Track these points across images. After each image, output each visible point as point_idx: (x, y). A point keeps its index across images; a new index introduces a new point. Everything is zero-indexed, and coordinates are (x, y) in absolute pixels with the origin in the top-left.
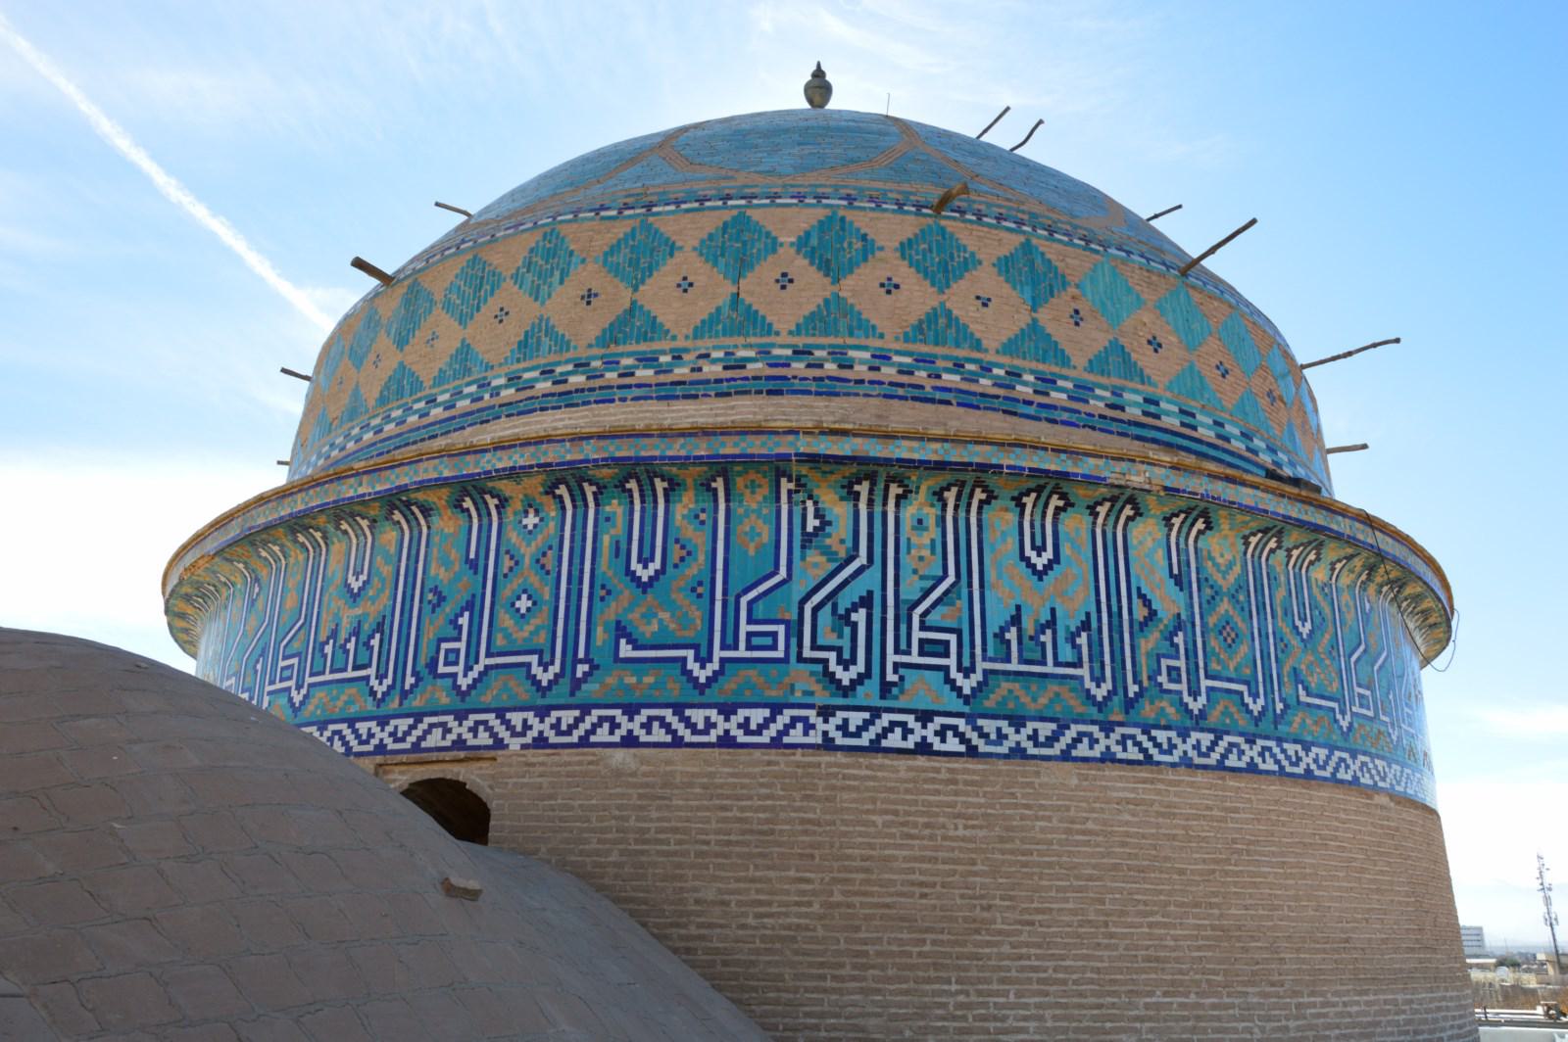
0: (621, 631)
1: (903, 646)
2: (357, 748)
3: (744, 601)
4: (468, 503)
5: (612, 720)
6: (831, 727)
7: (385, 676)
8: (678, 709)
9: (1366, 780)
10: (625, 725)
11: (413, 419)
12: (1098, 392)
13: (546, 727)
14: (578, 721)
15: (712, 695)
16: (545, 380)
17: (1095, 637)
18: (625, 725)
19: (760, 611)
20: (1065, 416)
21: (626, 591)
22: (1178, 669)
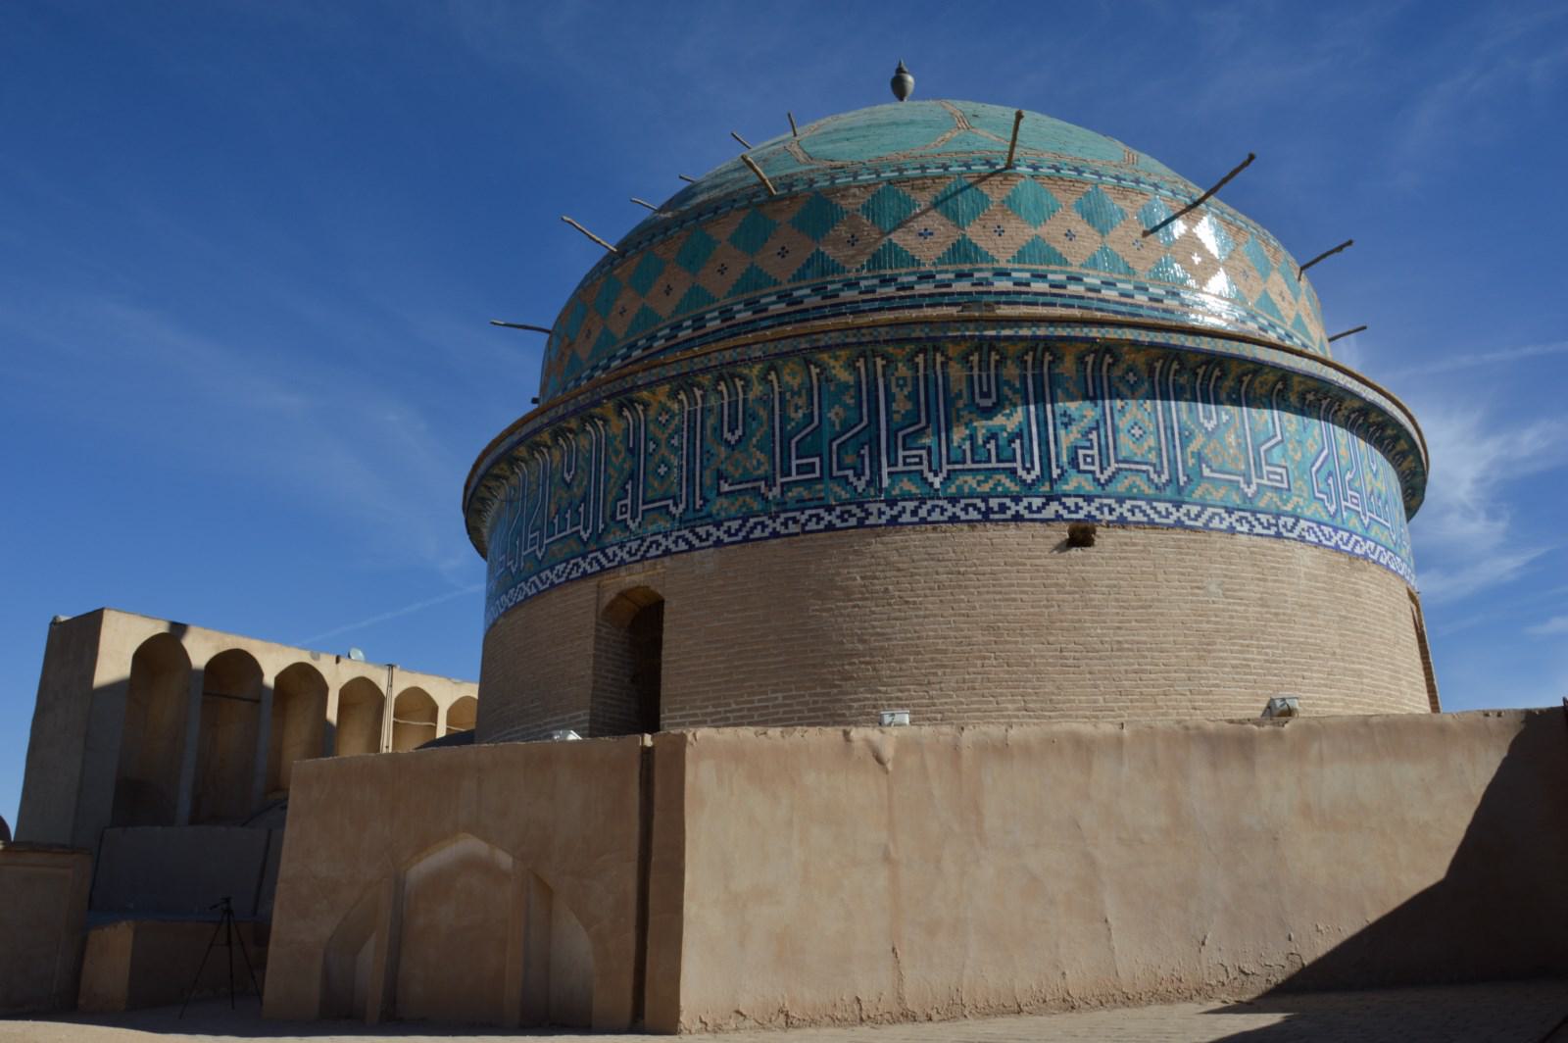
0: (720, 476)
1: (917, 460)
2: (608, 565)
5: (730, 535)
6: (1119, 510)
7: (637, 517)
8: (1149, 500)
9: (1392, 567)
10: (1021, 508)
12: (660, 334)
15: (1109, 489)
16: (816, 295)
17: (1027, 444)
21: (723, 451)
22: (1092, 457)
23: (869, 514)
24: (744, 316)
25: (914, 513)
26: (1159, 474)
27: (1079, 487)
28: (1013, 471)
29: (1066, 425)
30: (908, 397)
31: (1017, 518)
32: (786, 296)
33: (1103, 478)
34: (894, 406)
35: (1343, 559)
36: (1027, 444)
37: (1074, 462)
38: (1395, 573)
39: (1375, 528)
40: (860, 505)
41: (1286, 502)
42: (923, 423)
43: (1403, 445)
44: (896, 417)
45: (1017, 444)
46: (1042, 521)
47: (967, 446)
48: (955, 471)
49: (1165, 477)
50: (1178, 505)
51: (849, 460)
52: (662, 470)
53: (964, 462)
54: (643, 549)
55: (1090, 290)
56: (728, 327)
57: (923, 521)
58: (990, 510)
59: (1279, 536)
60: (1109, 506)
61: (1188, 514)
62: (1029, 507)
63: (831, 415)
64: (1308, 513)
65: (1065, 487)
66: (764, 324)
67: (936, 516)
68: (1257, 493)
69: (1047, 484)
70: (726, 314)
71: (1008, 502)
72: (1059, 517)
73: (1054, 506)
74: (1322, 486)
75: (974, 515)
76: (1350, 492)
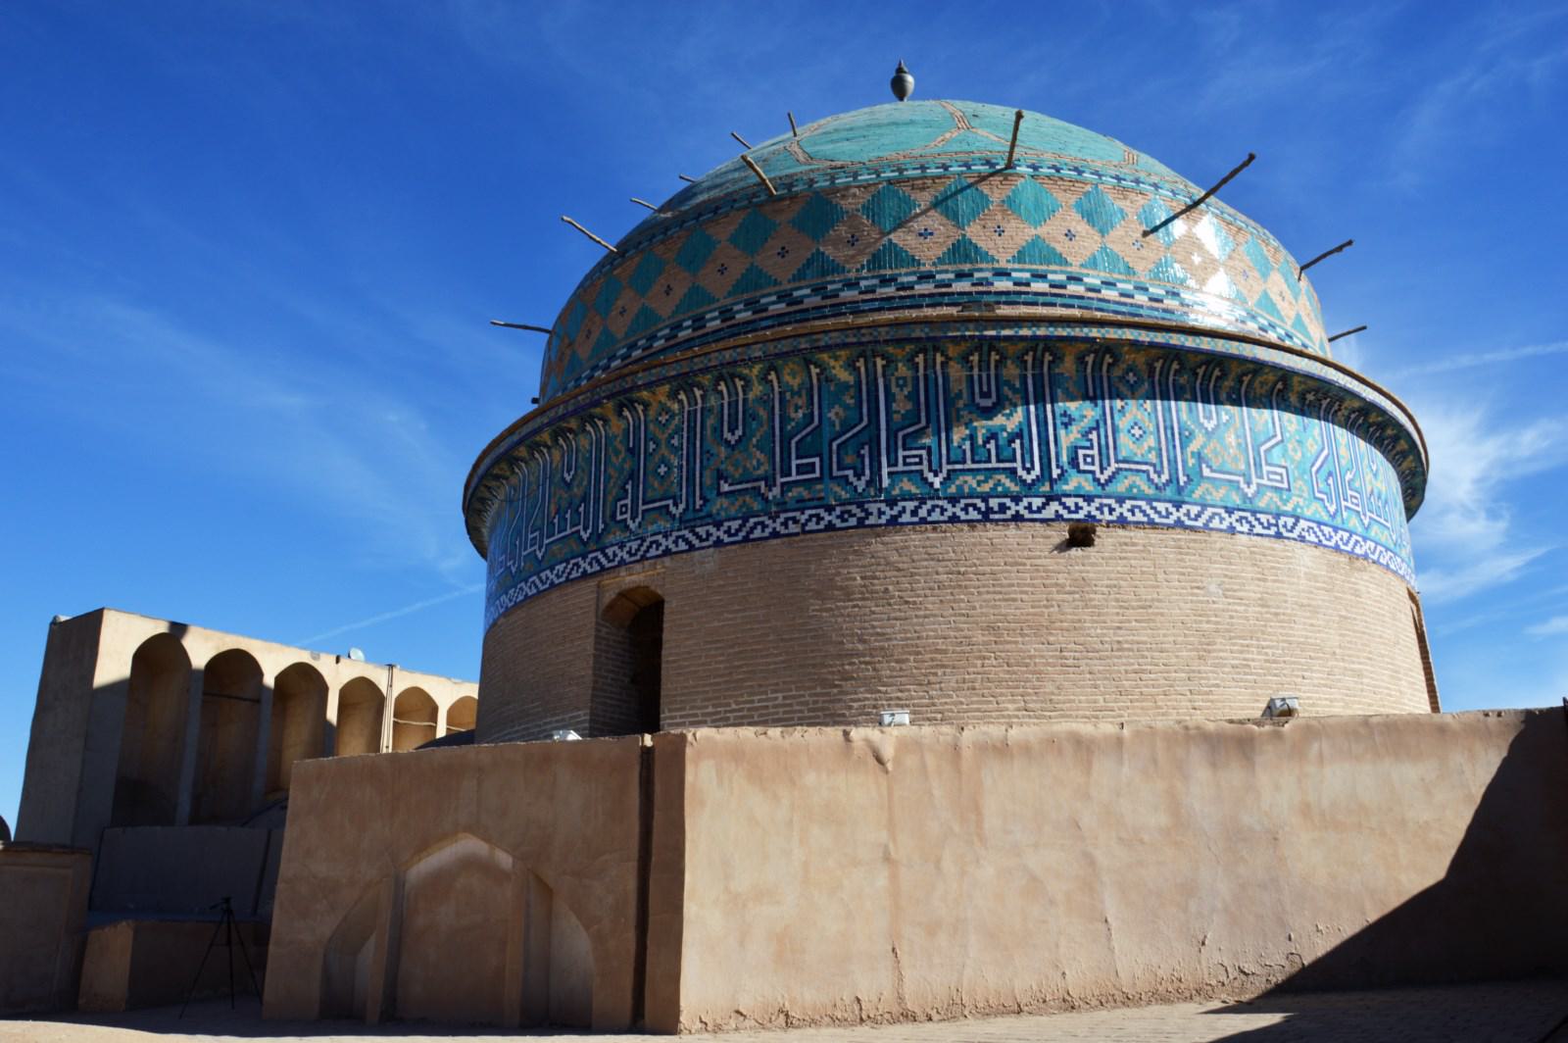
1: (917, 460)
7: (637, 517)
8: (1149, 500)
9: (1392, 566)
12: (660, 334)
15: (1109, 489)
17: (1027, 444)
22: (1092, 457)
23: (869, 514)
24: (744, 316)
25: (914, 513)
26: (1159, 474)
27: (1079, 487)
28: (1013, 471)
29: (1066, 425)
31: (1017, 518)
32: (786, 296)
33: (1103, 478)
35: (1343, 559)
36: (1027, 444)
37: (1074, 462)
38: (1395, 572)
39: (1375, 527)
40: (860, 505)
41: (1286, 502)
45: (1017, 444)
47: (967, 446)
48: (955, 471)
49: (1165, 477)
50: (1178, 506)
51: (848, 460)
52: (662, 470)
53: (964, 462)
54: (643, 548)
57: (923, 521)
58: (990, 510)
59: (1279, 536)
60: (1109, 506)
61: (1188, 514)
62: (1029, 507)
63: (832, 415)
64: (1308, 513)
65: (1065, 487)
67: (936, 516)
68: (1257, 492)
69: (1047, 484)
70: (726, 314)
72: (1058, 517)
73: (1054, 506)
74: (1322, 486)
75: (974, 515)
76: (1349, 492)
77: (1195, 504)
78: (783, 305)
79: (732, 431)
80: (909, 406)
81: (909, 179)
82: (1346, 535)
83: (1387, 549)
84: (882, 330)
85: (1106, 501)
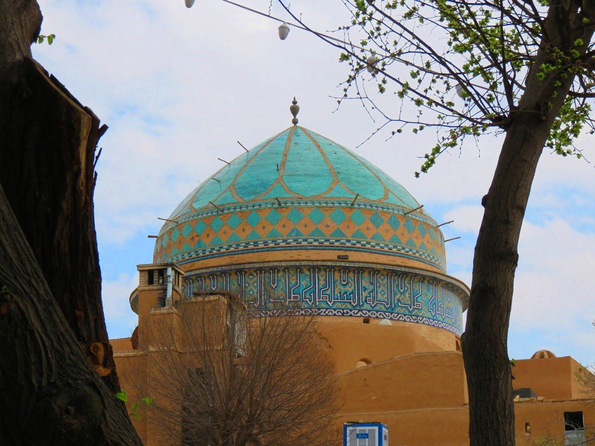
0: (399, 301)
3: (292, 290)
4: (187, 281)
8: (384, 312)
9: (451, 330)
11: (428, 258)
12: (241, 245)
13: (352, 313)
14: (397, 316)
15: (375, 308)
17: (354, 295)
18: (303, 312)
19: (294, 292)
20: (217, 255)
23: (313, 312)
24: (272, 245)
25: (325, 312)
26: (387, 304)
27: (367, 308)
28: (350, 303)
29: (364, 290)
30: (324, 280)
31: (351, 315)
32: (285, 241)
34: (320, 282)
35: (435, 329)
36: (354, 295)
37: (366, 301)
38: (452, 332)
39: (447, 318)
40: (311, 309)
41: (420, 313)
42: (328, 288)
43: (460, 291)
44: (321, 285)
45: (352, 295)
46: (357, 316)
47: (339, 295)
48: (336, 302)
49: (389, 306)
50: (391, 314)
51: (307, 297)
52: (251, 293)
53: (344, 299)
55: (372, 247)
56: (267, 248)
57: (327, 315)
58: (344, 313)
59: (417, 322)
60: (374, 313)
61: (394, 316)
62: (354, 313)
63: (303, 283)
64: (426, 316)
65: (363, 308)
66: (278, 249)
67: (330, 314)
70: (266, 243)
71: (349, 311)
72: (361, 316)
73: (360, 313)
74: (432, 308)
75: (340, 314)
76: (439, 309)
77: (396, 313)
78: (284, 244)
79: (274, 284)
80: (324, 283)
81: (323, 207)
82: (437, 322)
83: (450, 325)
84: (319, 262)
85: (373, 312)
